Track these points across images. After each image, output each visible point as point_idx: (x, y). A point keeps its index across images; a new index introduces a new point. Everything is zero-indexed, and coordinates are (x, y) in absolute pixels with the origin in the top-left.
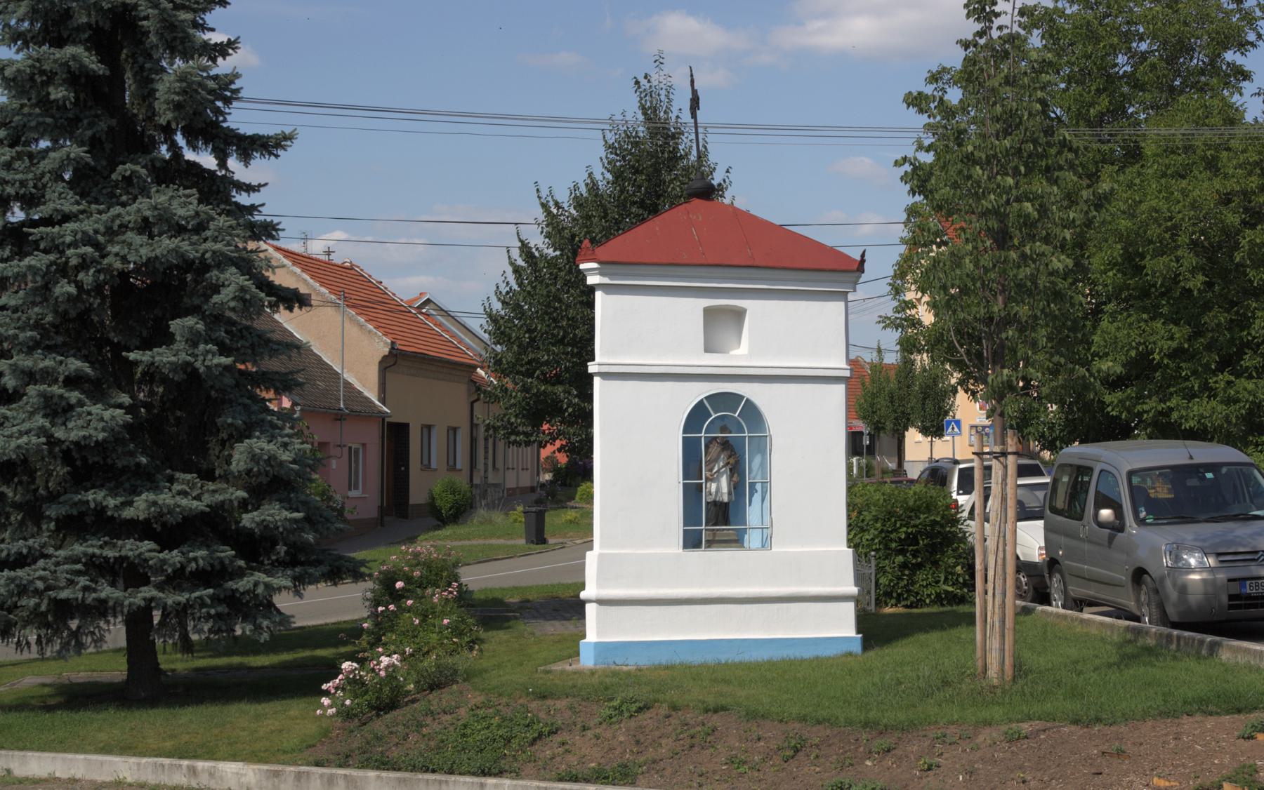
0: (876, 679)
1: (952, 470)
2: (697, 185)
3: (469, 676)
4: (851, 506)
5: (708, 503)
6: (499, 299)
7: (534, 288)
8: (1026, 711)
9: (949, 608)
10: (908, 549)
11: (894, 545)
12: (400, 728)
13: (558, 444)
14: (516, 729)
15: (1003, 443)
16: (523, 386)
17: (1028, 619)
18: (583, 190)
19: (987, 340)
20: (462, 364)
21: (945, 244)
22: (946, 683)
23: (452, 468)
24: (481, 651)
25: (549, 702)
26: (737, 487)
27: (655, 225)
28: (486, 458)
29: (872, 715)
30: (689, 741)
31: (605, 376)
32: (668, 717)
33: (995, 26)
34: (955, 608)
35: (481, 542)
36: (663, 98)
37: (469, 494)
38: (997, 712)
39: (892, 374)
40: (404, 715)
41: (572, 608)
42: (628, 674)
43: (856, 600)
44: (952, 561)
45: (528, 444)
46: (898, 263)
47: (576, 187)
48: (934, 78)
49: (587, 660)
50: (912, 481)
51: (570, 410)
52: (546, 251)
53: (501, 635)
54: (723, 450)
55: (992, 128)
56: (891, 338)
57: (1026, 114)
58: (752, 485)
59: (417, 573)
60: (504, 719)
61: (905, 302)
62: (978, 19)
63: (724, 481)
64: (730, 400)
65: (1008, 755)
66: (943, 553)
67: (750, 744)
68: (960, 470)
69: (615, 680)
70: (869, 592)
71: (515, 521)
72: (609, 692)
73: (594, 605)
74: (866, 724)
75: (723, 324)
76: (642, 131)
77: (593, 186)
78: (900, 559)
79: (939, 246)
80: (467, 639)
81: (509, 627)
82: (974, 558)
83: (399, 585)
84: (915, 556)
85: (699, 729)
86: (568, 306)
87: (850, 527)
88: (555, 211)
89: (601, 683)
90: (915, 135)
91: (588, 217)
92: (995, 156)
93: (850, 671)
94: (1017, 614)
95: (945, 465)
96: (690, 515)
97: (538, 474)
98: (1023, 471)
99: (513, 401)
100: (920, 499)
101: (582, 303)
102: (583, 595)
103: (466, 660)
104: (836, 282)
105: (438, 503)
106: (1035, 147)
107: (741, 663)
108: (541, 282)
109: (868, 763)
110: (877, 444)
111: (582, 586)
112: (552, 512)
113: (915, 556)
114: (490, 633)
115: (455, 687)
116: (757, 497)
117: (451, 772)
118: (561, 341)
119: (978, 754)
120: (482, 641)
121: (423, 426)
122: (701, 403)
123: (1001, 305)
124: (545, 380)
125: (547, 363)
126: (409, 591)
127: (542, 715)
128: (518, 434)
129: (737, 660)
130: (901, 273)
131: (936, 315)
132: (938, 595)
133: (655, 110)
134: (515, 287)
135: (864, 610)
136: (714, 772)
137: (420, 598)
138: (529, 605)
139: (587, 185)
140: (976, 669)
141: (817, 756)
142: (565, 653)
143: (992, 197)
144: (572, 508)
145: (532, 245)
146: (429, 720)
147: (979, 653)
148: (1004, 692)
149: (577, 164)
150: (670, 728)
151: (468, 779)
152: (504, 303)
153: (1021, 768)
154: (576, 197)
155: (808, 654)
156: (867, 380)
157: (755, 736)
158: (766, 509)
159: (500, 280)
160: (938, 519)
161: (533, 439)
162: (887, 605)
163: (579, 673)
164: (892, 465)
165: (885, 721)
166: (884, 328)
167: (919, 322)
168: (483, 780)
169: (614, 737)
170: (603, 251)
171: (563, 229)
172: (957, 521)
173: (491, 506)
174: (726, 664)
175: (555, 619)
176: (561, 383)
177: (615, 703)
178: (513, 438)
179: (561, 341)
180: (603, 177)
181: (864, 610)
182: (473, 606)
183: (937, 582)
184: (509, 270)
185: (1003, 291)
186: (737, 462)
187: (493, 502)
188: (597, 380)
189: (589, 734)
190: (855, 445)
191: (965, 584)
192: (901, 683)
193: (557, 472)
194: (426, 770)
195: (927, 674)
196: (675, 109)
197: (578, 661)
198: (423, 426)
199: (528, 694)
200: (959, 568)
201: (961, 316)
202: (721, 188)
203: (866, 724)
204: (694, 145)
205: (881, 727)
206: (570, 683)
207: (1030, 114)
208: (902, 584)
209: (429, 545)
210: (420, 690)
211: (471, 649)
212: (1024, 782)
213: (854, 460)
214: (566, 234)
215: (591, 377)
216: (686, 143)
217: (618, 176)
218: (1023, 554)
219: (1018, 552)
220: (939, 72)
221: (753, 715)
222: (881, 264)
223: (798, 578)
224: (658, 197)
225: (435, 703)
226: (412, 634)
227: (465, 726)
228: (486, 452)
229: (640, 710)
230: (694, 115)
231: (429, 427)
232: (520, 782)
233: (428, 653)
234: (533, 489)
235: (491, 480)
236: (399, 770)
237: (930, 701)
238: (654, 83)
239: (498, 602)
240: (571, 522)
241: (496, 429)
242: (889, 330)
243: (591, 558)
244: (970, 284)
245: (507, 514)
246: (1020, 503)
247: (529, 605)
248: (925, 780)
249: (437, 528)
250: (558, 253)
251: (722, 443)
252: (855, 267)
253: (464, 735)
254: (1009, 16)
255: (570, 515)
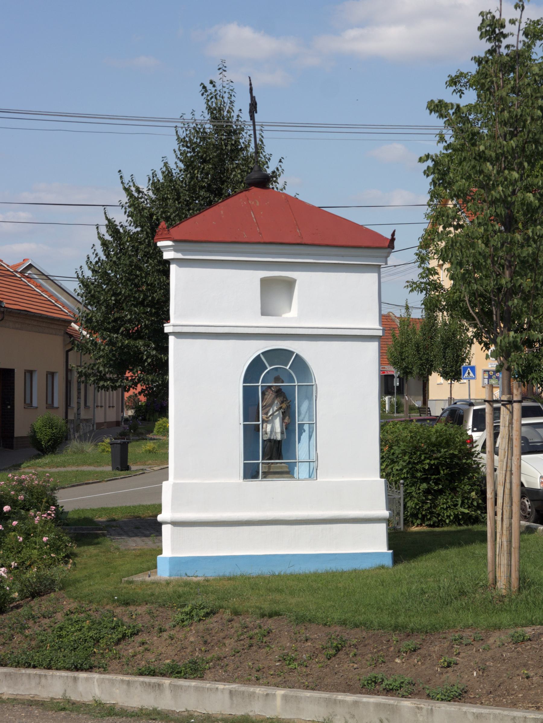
0: (404, 590)
1: (468, 411)
2: (255, 175)
3: (64, 585)
4: (383, 442)
5: (264, 441)
6: (90, 268)
7: (119, 259)
8: (529, 617)
9: (465, 527)
10: (432, 478)
11: (419, 474)
12: (7, 630)
13: (139, 388)
14: (104, 631)
15: (510, 393)
16: (110, 340)
17: (531, 536)
18: (160, 177)
19: (497, 307)
20: (59, 320)
21: (461, 226)
22: (463, 593)
23: (50, 406)
24: (74, 564)
25: (132, 608)
26: (288, 428)
27: (221, 209)
28: (79, 398)
29: (401, 620)
30: (248, 641)
31: (179, 335)
32: (230, 621)
33: (503, 44)
34: (470, 527)
35: (74, 468)
36: (226, 100)
37: (64, 429)
38: (505, 618)
39: (418, 327)
40: (10, 619)
41: (148, 525)
42: (198, 584)
43: (388, 521)
44: (467, 487)
45: (114, 388)
46: (423, 237)
47: (154, 175)
48: (453, 81)
49: (163, 572)
50: (436, 420)
51: (149, 360)
52: (128, 228)
53: (92, 550)
54: (277, 397)
55: (500, 130)
56: (417, 299)
57: (529, 119)
58: (301, 426)
59: (21, 497)
60: (93, 623)
61: (428, 269)
62: (489, 40)
63: (277, 422)
64: (281, 355)
65: (515, 654)
66: (460, 481)
67: (299, 644)
68: (474, 410)
69: (186, 589)
70: (398, 514)
71: (103, 451)
72: (182, 599)
73: (169, 526)
74: (396, 628)
75: (275, 291)
76: (209, 127)
77: (168, 174)
78: (424, 486)
79: (456, 228)
80: (63, 555)
81: (98, 543)
82: (485, 485)
83: (6, 508)
84: (436, 484)
85: (257, 631)
86: (147, 274)
87: (383, 459)
88: (136, 195)
89: (175, 592)
90: (438, 132)
91: (165, 199)
92: (503, 154)
93: (383, 582)
94: (521, 533)
95: (462, 407)
96: (249, 451)
97: (122, 411)
98: (526, 412)
99: (101, 353)
100: (441, 436)
101: (159, 271)
102: (160, 518)
103: (61, 571)
104: (373, 257)
105: (39, 436)
106: (536, 147)
107: (291, 575)
108: (124, 254)
109: (398, 661)
110: (406, 386)
111: (158, 509)
112: (134, 443)
113: (436, 484)
114: (82, 549)
115: (52, 595)
116: (305, 436)
117: (49, 668)
118: (142, 303)
119: (489, 654)
120: (75, 555)
121: (26, 372)
122: (258, 358)
123: (508, 279)
124: (128, 335)
125: (130, 321)
126: (14, 513)
127: (126, 619)
128: (106, 380)
129: (288, 572)
130: (425, 244)
131: (454, 280)
132: (456, 516)
133: (220, 110)
134: (103, 258)
135: (394, 528)
136: (269, 668)
137: (21, 519)
138: (114, 523)
139: (163, 173)
140: (487, 581)
141: (355, 655)
142: (145, 566)
143: (500, 188)
144: (151, 439)
145: (117, 223)
146: (31, 623)
147: (490, 567)
148: (511, 600)
149: (155, 155)
150: (233, 631)
151: (64, 673)
152: (94, 271)
153: (525, 665)
154: (153, 183)
155: (347, 566)
156: (397, 332)
157: (303, 638)
158: (313, 446)
159: (90, 252)
160: (456, 453)
161: (118, 384)
162: (413, 524)
163: (156, 583)
164: (418, 404)
165: (411, 625)
166: (412, 291)
167: (441, 287)
168: (76, 674)
169: (186, 638)
170: (179, 231)
171: (143, 209)
172: (472, 454)
173: (83, 438)
174: (279, 575)
175: (136, 535)
176: (141, 338)
177: (187, 609)
178: (101, 383)
179: (142, 303)
180: (176, 166)
181: (394, 528)
182: (67, 525)
183: (456, 505)
184: (98, 243)
185: (510, 266)
186: (288, 407)
187: (85, 434)
188: (171, 339)
189: (165, 635)
190: (387, 385)
191: (479, 507)
192: (425, 593)
193: (138, 409)
194: (28, 665)
195: (447, 585)
196: (236, 109)
197: (156, 572)
198: (26, 372)
199: (114, 601)
200: (473, 494)
201: (475, 287)
202: (275, 175)
203: (396, 628)
204: (253, 139)
205: (409, 630)
206: (149, 592)
207: (532, 119)
208: (426, 507)
209: (33, 472)
210: (23, 597)
211: (66, 563)
212: (528, 677)
213: (387, 399)
214: (146, 213)
215: (167, 336)
216: (246, 137)
217: (189, 165)
218: (527, 482)
219: (523, 480)
220: (457, 77)
221: (302, 620)
222: (409, 238)
223: (339, 503)
224: (223, 183)
225: (36, 608)
226: (18, 549)
227: (61, 629)
228: (79, 393)
229: (207, 615)
230: (252, 118)
231: (31, 372)
232: (107, 676)
233: (30, 565)
234: (118, 424)
235: (83, 416)
236: (6, 665)
237: (449, 607)
238: (219, 88)
239: (88, 521)
240: (150, 451)
241: (87, 376)
242: (415, 292)
243: (167, 487)
244: (482, 261)
245: (96, 445)
246: (524, 439)
247: (114, 523)
248: (445, 676)
249: (38, 457)
250: (139, 229)
251: (275, 391)
252: (387, 244)
253: (60, 636)
254: (515, 37)
255: (150, 445)
